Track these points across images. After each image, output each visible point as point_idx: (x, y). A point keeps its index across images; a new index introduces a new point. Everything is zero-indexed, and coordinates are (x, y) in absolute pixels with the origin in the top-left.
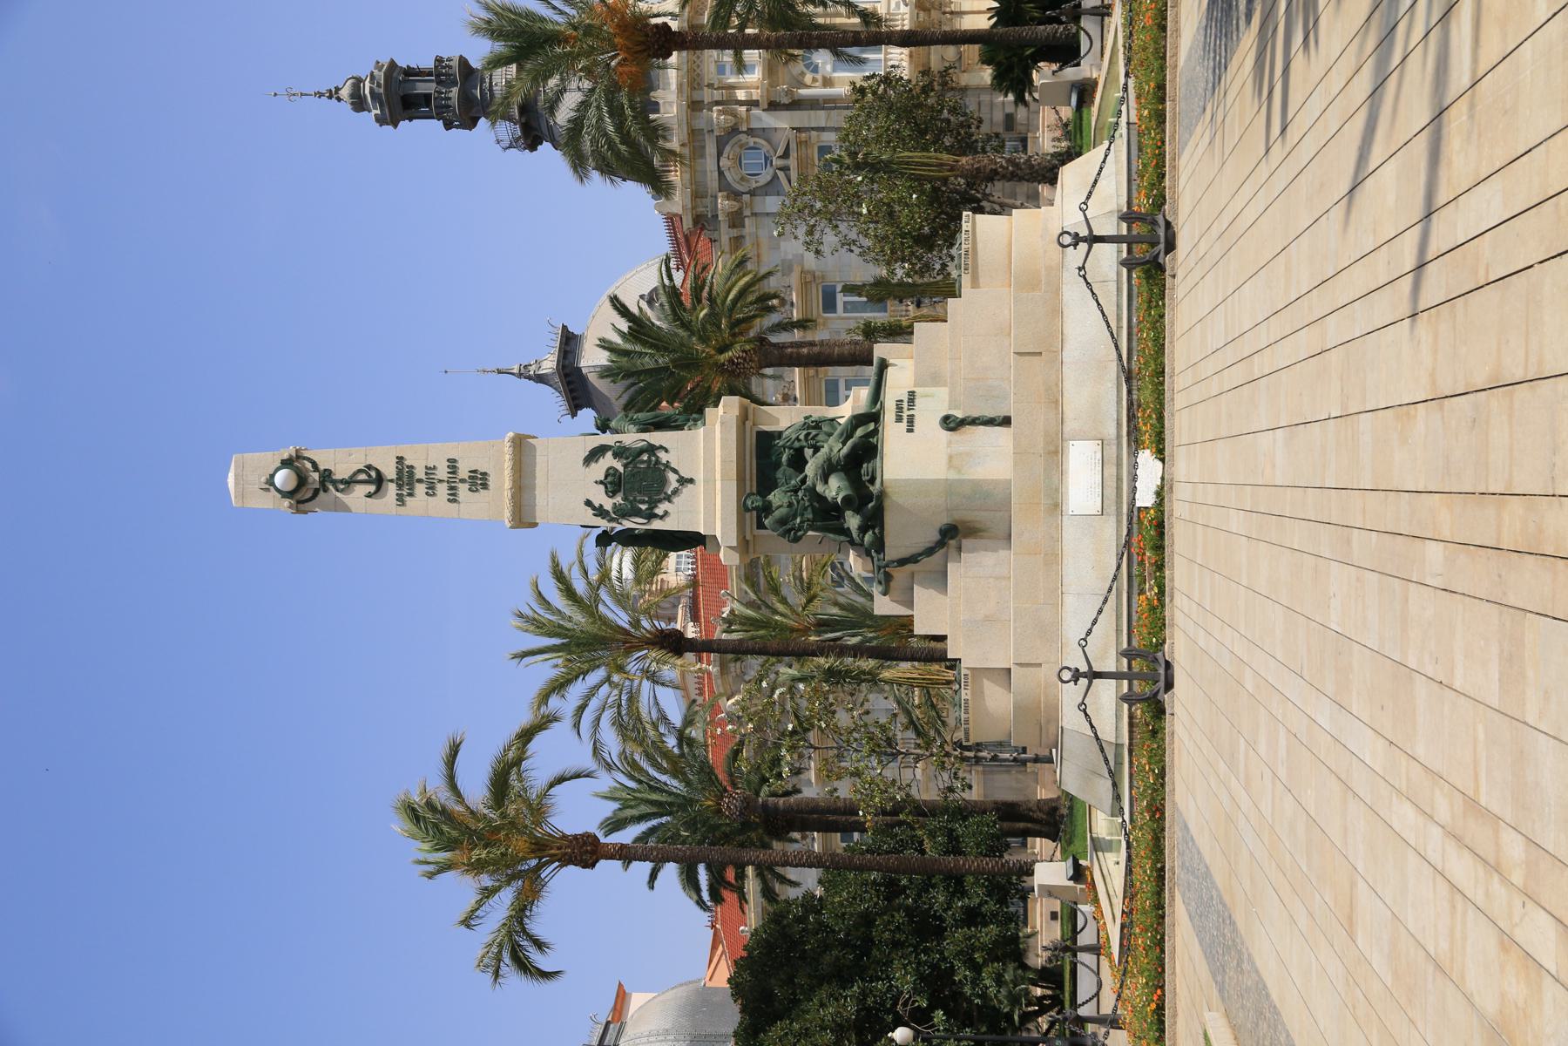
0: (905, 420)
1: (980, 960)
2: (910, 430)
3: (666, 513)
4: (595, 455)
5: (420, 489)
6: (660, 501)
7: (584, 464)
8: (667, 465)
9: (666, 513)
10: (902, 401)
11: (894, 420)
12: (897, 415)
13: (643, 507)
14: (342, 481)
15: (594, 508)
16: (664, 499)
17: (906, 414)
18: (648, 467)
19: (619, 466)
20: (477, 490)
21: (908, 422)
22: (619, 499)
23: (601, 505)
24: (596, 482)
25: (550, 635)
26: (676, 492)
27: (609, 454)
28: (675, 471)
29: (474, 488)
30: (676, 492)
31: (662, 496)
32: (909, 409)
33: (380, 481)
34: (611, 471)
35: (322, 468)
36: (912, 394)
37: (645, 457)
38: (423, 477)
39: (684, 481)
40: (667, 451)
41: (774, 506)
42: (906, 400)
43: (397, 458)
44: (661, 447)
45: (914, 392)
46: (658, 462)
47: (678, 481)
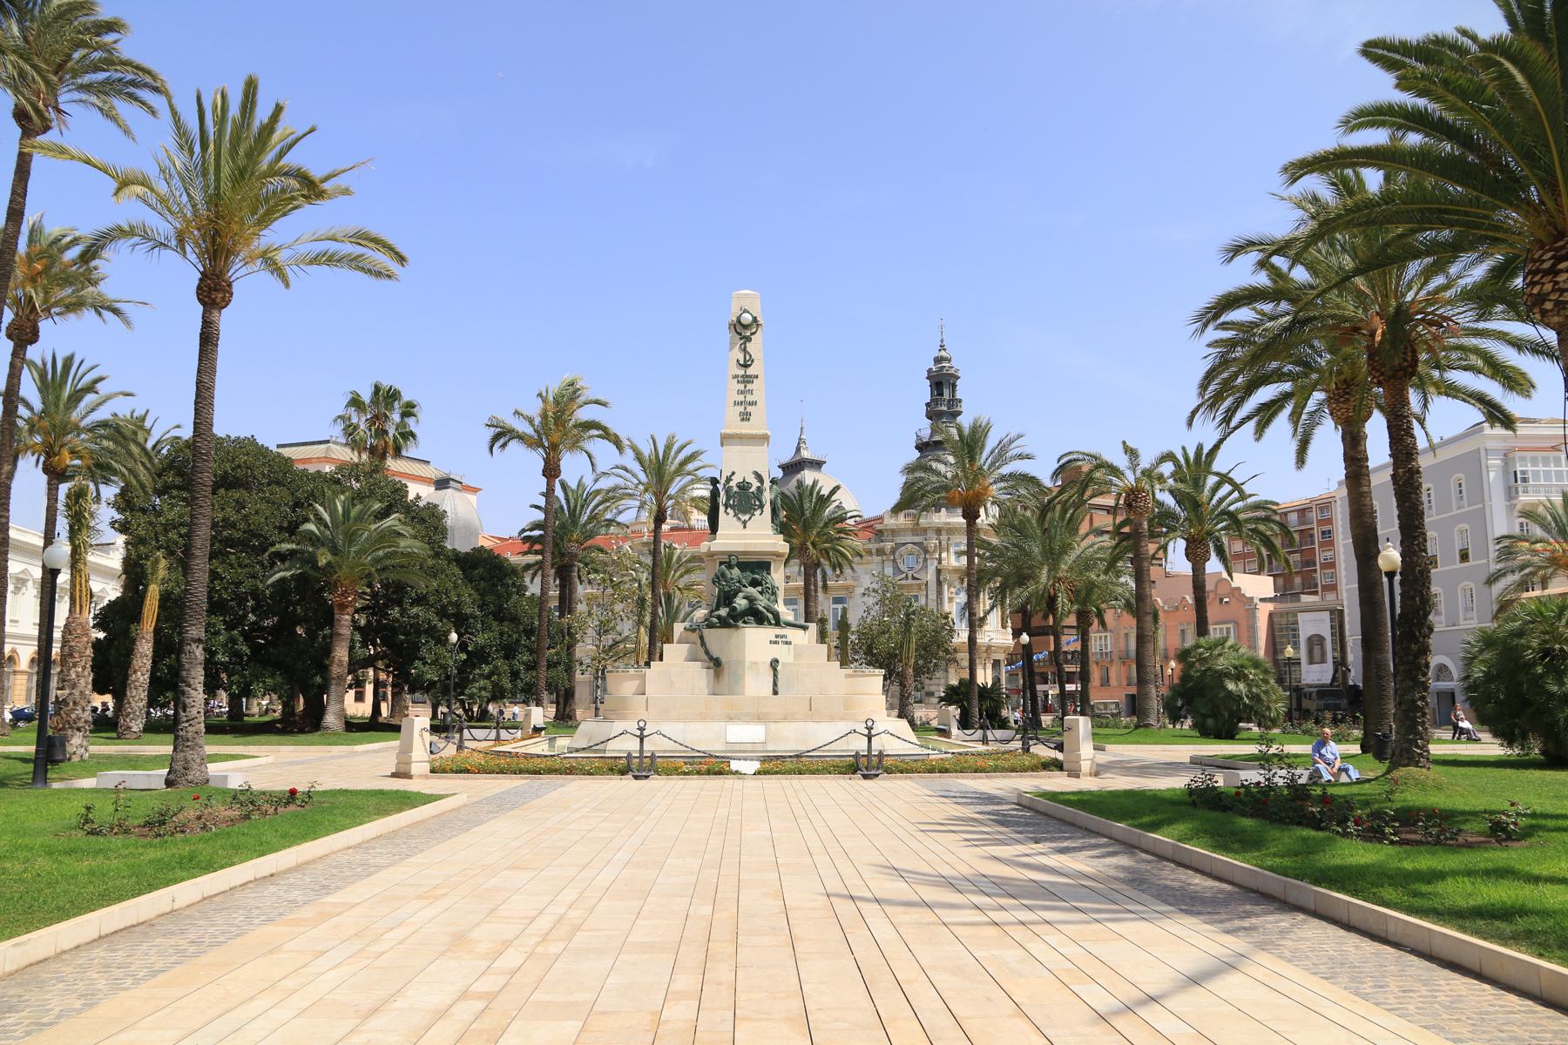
5: (741, 387)
8: (753, 515)
13: (731, 502)
26: (739, 519)
30: (739, 519)
33: (746, 366)
36: (790, 643)
37: (757, 503)
39: (745, 523)
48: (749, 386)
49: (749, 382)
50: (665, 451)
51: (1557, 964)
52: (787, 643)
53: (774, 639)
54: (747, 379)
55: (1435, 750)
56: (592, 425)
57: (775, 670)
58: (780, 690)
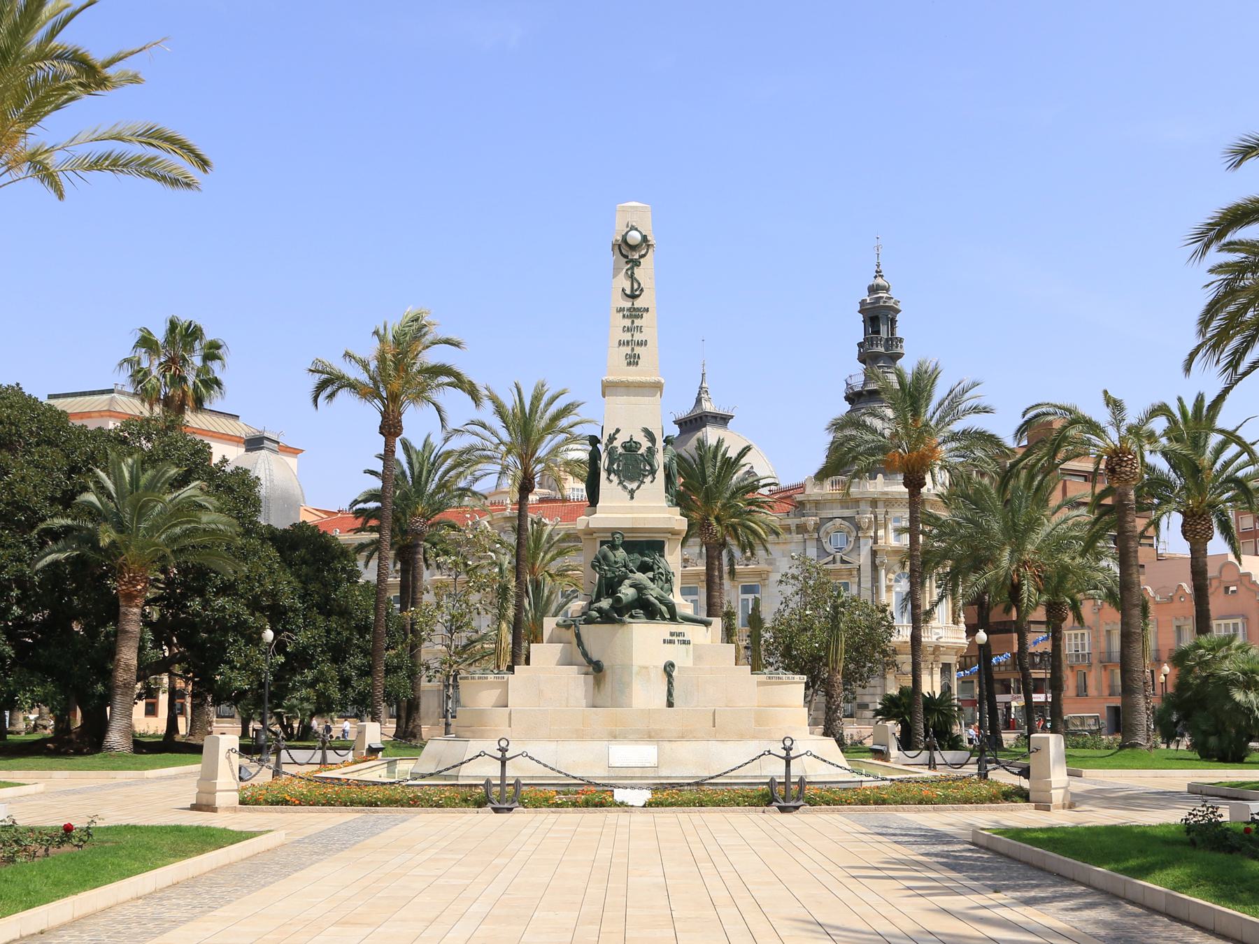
0: (671, 638)
3: (611, 481)
5: (628, 322)
6: (619, 477)
8: (642, 482)
15: (614, 434)
19: (642, 451)
22: (620, 450)
26: (625, 487)
30: (625, 487)
31: (622, 479)
33: (633, 297)
36: (689, 643)
38: (635, 325)
39: (632, 492)
44: (654, 478)
46: (645, 476)
57: (670, 676)
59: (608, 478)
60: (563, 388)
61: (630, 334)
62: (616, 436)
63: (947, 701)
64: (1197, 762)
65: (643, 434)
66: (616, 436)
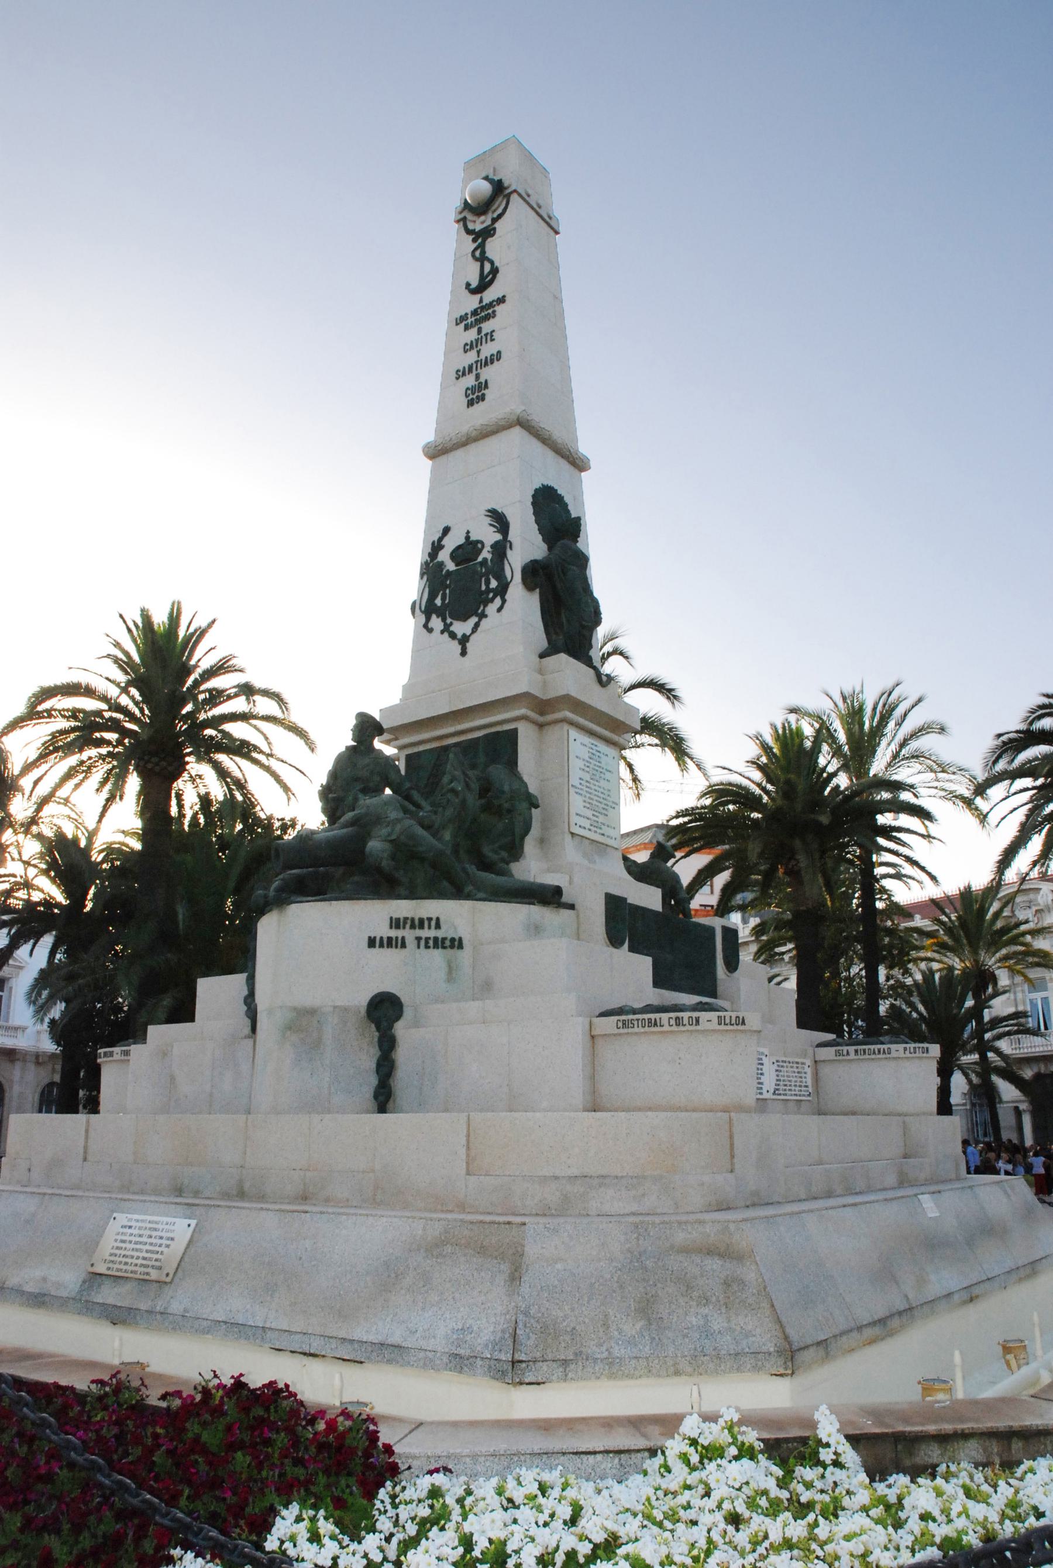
0: (393, 933)
1: (913, 1013)
2: (372, 943)
3: (430, 631)
4: (500, 520)
5: (472, 335)
6: (444, 620)
7: (489, 511)
8: (483, 616)
9: (430, 631)
10: (438, 926)
11: (395, 916)
12: (406, 919)
13: (438, 602)
14: (483, 252)
15: (440, 539)
16: (445, 624)
17: (409, 935)
18: (482, 593)
19: (486, 554)
20: (467, 396)
21: (390, 939)
22: (451, 566)
23: (444, 546)
24: (468, 532)
25: (895, 837)
26: (453, 636)
27: (498, 537)
28: (477, 626)
29: (469, 392)
30: (453, 636)
31: (449, 621)
32: (419, 939)
33: (483, 285)
34: (479, 546)
35: (496, 225)
36: (457, 944)
37: (494, 584)
38: (475, 330)
39: (464, 641)
40: (499, 610)
41: (664, 832)
42: (440, 934)
43: (504, 296)
44: (504, 601)
45: (461, 946)
46: (488, 602)
47: (464, 635)
48: (486, 327)
49: (487, 318)
50: (899, 839)
51: (505, 712)
52: (438, 943)
53: (384, 931)
54: (483, 314)
55: (21, 903)
56: (649, 726)
57: (387, 1044)
58: (89, 1158)
59: (426, 626)
60: (769, 726)
61: (474, 353)
62: (443, 543)
63: (769, 876)
64: (581, 915)
65: (488, 520)
66: (443, 543)
